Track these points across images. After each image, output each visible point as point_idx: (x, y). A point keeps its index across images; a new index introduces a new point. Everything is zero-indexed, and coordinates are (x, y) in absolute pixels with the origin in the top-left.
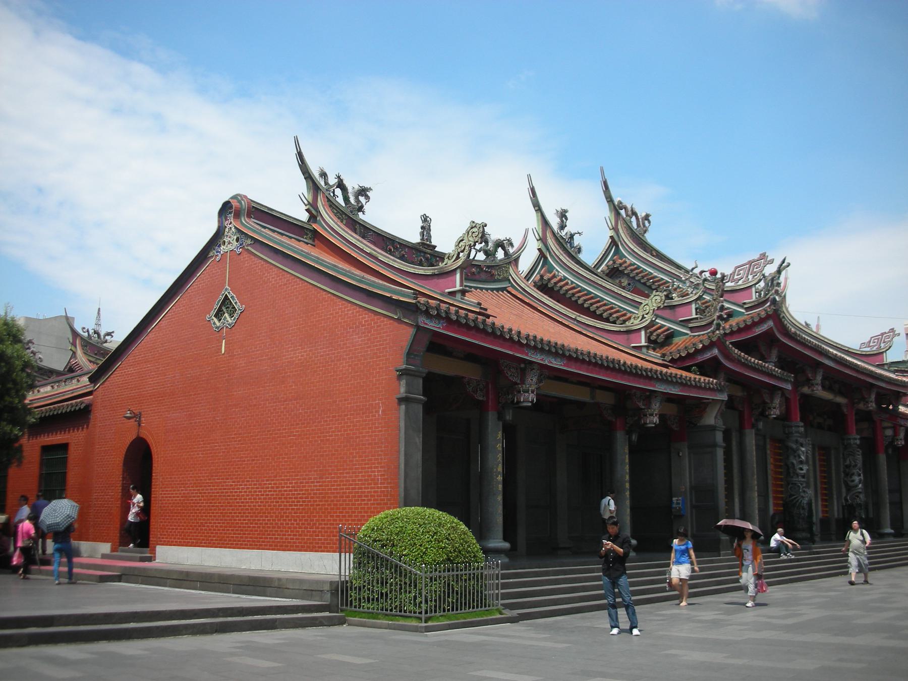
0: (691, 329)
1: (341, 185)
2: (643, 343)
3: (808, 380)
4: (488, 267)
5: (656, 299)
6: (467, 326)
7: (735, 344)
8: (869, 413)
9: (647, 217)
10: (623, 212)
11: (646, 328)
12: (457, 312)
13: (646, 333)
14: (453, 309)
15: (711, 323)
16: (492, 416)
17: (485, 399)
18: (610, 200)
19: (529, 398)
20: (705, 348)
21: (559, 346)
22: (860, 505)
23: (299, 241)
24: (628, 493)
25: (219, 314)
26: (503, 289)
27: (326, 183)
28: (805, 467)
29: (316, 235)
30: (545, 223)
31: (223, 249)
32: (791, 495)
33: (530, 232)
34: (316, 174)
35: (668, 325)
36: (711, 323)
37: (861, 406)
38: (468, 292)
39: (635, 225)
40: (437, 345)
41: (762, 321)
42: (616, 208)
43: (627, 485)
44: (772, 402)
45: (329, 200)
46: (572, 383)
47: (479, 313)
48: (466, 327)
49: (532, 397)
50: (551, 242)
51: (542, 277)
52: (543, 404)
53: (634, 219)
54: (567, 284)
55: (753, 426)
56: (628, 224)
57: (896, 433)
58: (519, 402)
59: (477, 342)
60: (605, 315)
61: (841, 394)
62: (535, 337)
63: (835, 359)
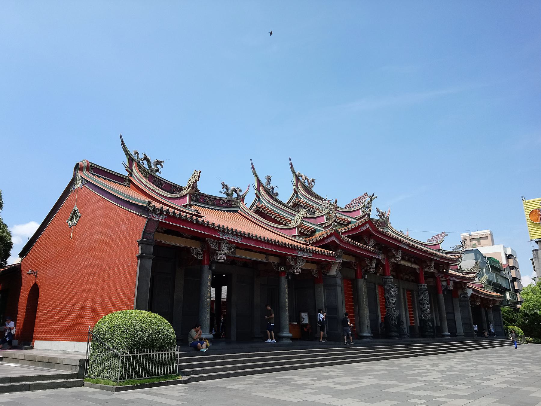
0: (324, 228)
1: (146, 159)
3: (428, 266)
5: (302, 213)
6: (186, 220)
8: (433, 273)
9: (313, 181)
10: (300, 178)
11: (298, 227)
12: (174, 212)
13: (298, 230)
14: (189, 216)
15: (331, 224)
16: (206, 267)
17: (202, 259)
18: (294, 172)
19: (222, 258)
20: (328, 236)
21: (238, 231)
22: (428, 320)
23: (121, 184)
24: (287, 308)
26: (236, 212)
28: (394, 299)
29: (130, 182)
30: (259, 181)
31: (76, 187)
32: (388, 313)
33: (251, 187)
35: (313, 226)
36: (331, 224)
37: (427, 269)
41: (363, 225)
42: (297, 177)
43: (287, 304)
44: (371, 265)
45: (138, 166)
46: (242, 249)
47: (195, 215)
48: (186, 221)
49: (300, 271)
50: (262, 190)
51: (257, 206)
52: (232, 261)
53: (306, 181)
54: (268, 209)
55: (362, 277)
56: (304, 185)
57: (448, 284)
59: (187, 228)
60: (284, 223)
61: (415, 263)
62: (223, 226)
63: (408, 245)
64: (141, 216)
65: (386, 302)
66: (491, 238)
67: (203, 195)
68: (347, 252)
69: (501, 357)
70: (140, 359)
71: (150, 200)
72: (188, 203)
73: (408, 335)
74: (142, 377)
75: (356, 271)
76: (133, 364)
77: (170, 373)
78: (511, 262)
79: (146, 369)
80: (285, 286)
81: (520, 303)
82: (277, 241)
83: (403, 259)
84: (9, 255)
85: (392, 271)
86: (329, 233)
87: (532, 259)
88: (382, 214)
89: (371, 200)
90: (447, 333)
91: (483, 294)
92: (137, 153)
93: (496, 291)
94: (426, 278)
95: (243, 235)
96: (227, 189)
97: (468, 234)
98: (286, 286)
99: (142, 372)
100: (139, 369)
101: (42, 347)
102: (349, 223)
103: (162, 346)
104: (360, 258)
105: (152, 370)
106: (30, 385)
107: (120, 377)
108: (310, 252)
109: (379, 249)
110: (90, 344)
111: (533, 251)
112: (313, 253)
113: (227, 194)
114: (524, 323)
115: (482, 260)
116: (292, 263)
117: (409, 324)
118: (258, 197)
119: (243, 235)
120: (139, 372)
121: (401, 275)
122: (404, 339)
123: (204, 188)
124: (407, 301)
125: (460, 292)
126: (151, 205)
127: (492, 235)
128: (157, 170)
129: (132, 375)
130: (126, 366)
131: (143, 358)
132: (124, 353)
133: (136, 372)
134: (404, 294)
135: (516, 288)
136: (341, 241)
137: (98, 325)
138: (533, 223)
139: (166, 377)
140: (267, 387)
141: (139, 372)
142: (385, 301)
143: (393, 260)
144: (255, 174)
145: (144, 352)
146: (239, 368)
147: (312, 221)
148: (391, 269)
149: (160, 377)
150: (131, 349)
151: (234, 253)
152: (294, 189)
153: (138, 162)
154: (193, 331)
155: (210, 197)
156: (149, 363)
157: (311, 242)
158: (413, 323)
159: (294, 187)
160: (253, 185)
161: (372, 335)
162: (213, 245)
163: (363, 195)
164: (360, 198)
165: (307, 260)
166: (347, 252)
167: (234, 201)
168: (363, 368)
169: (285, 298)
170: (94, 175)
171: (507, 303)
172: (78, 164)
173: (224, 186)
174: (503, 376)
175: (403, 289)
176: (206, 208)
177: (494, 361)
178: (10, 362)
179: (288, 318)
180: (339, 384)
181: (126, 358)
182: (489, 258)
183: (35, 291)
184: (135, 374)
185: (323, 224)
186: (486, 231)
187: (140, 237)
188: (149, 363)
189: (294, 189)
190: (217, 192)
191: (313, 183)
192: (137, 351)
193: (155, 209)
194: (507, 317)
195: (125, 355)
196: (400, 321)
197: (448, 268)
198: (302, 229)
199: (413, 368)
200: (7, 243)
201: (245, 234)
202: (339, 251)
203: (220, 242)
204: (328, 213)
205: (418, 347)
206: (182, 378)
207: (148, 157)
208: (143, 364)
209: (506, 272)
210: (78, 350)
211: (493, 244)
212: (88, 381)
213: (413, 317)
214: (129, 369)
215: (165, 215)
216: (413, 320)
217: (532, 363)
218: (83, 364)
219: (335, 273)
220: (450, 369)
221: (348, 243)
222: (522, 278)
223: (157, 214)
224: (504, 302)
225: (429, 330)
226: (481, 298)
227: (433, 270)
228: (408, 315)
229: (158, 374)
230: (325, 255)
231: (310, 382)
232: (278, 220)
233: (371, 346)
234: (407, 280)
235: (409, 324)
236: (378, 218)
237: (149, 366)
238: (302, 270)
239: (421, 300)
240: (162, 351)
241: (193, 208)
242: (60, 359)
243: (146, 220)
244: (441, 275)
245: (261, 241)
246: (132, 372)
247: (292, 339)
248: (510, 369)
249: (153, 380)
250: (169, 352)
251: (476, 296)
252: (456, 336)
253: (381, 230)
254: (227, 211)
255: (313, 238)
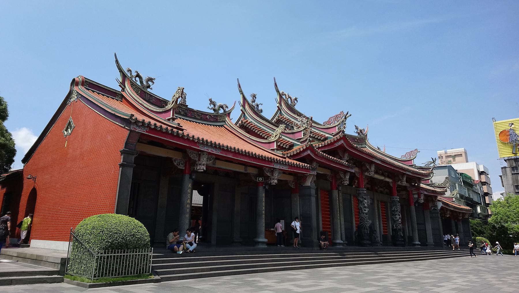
0: (301, 142)
1: (138, 76)
2: (275, 148)
3: (400, 180)
4: (214, 116)
7: (322, 151)
8: (405, 187)
9: (296, 99)
10: (284, 97)
11: (277, 141)
16: (187, 176)
17: (184, 168)
18: (278, 91)
19: (202, 168)
20: (304, 151)
23: (113, 99)
24: (264, 216)
25: (66, 130)
26: (222, 126)
27: (131, 74)
28: (367, 210)
29: (122, 97)
30: (244, 99)
32: (361, 223)
33: (237, 103)
34: (125, 70)
35: (291, 141)
37: (399, 183)
38: (176, 119)
39: (290, 102)
40: (142, 139)
41: (338, 140)
42: (281, 97)
43: (264, 212)
45: (131, 82)
48: (166, 133)
49: (276, 181)
50: (247, 107)
51: (242, 121)
52: (211, 171)
53: (289, 99)
56: (287, 103)
58: (271, 183)
60: (265, 137)
61: (388, 177)
62: (203, 139)
64: (124, 128)
65: (359, 212)
66: (465, 156)
67: (192, 110)
68: (322, 165)
69: (463, 265)
70: (114, 259)
71: (156, 122)
72: (171, 117)
73: (381, 243)
74: (115, 275)
75: (331, 183)
76: (107, 264)
77: (143, 273)
78: (483, 178)
79: (119, 268)
80: (262, 194)
81: (489, 216)
82: (254, 153)
83: (376, 172)
84: (13, 161)
85: (367, 184)
86: (305, 148)
87: (501, 176)
88: (361, 131)
89: (346, 118)
90: (262, 239)
91: (452, 206)
92: (130, 71)
93: (468, 205)
94: (398, 191)
95: (222, 148)
96: (215, 106)
97: (444, 151)
98: (264, 195)
99: (116, 270)
100: (113, 268)
101: (38, 246)
102: (326, 139)
103: (136, 248)
104: (335, 172)
105: (125, 269)
106: (12, 279)
107: (95, 275)
108: (286, 164)
109: (354, 164)
110: (72, 243)
111: (502, 168)
112: (288, 165)
113: (214, 110)
114: (491, 235)
115: (455, 175)
116: (268, 174)
117: (382, 233)
118: (243, 113)
119: (222, 148)
120: (113, 271)
121: (376, 188)
122: (376, 247)
123: (191, 104)
124: (380, 211)
125: (430, 205)
126: (134, 118)
127: (466, 153)
128: (149, 87)
129: (106, 274)
130: (100, 265)
131: (117, 259)
132: (99, 253)
133: (109, 270)
134: (378, 205)
135: (487, 202)
136: (316, 155)
137: (78, 227)
138: (502, 143)
139: (139, 276)
140: (230, 287)
141: (113, 271)
142: (359, 211)
143: (366, 174)
144: (241, 92)
145: (118, 253)
146: (211, 270)
147: (291, 136)
148: (365, 182)
149: (132, 276)
150: (106, 249)
151: (214, 163)
152: (278, 107)
153: (130, 79)
154: (171, 234)
155: (198, 112)
156: (123, 263)
157: (289, 155)
158: (387, 232)
159: (278, 105)
160: (239, 102)
161: (347, 242)
162: (193, 156)
163: (339, 113)
164: (337, 116)
165: (284, 172)
166: (322, 165)
167: (221, 116)
168: (328, 273)
169: (262, 206)
170: (89, 90)
171: (478, 216)
172: (74, 80)
173: (212, 102)
174: (455, 284)
175: (378, 201)
176: (193, 122)
177: (455, 269)
178: (5, 258)
179: (264, 225)
180: (298, 286)
181: (101, 258)
182: (461, 174)
183: (34, 193)
184: (109, 273)
185: (300, 139)
186: (461, 149)
187: (122, 147)
188: (123, 263)
189: (278, 107)
190: (205, 108)
191: (296, 101)
192: (112, 252)
193: (137, 122)
194: (476, 229)
195: (99, 255)
196: (372, 229)
197: (420, 183)
198: (281, 143)
199: (375, 273)
200: (11, 150)
201: (223, 146)
202: (315, 164)
203: (200, 153)
204: (305, 129)
205: (387, 255)
206: (153, 277)
207: (140, 74)
208: (117, 263)
209: (478, 187)
210: (58, 249)
211: (467, 161)
212: (68, 278)
213: (386, 227)
214: (103, 268)
215: (147, 127)
216: (386, 229)
217: (489, 272)
218: (64, 262)
219: (309, 185)
220: (409, 275)
221: (323, 157)
222: (493, 194)
223: (139, 127)
224: (474, 215)
225: (400, 239)
226: (451, 211)
227: (404, 183)
228: (382, 225)
229: (131, 273)
230: (300, 167)
231: (273, 284)
232: (261, 134)
233: (342, 253)
234: (381, 192)
235: (382, 233)
236: (357, 135)
237: (123, 266)
238: (278, 180)
239: (394, 211)
240: (136, 252)
241: (176, 122)
242: (46, 257)
243: (128, 132)
244: (413, 189)
245: (239, 153)
246: (106, 271)
247: (268, 244)
248: (465, 277)
249: (125, 278)
250: (137, 254)
251: (446, 207)
252: (427, 245)
253: (355, 146)
254: (214, 125)
255: (290, 151)
